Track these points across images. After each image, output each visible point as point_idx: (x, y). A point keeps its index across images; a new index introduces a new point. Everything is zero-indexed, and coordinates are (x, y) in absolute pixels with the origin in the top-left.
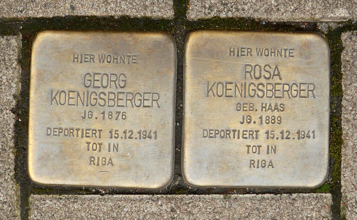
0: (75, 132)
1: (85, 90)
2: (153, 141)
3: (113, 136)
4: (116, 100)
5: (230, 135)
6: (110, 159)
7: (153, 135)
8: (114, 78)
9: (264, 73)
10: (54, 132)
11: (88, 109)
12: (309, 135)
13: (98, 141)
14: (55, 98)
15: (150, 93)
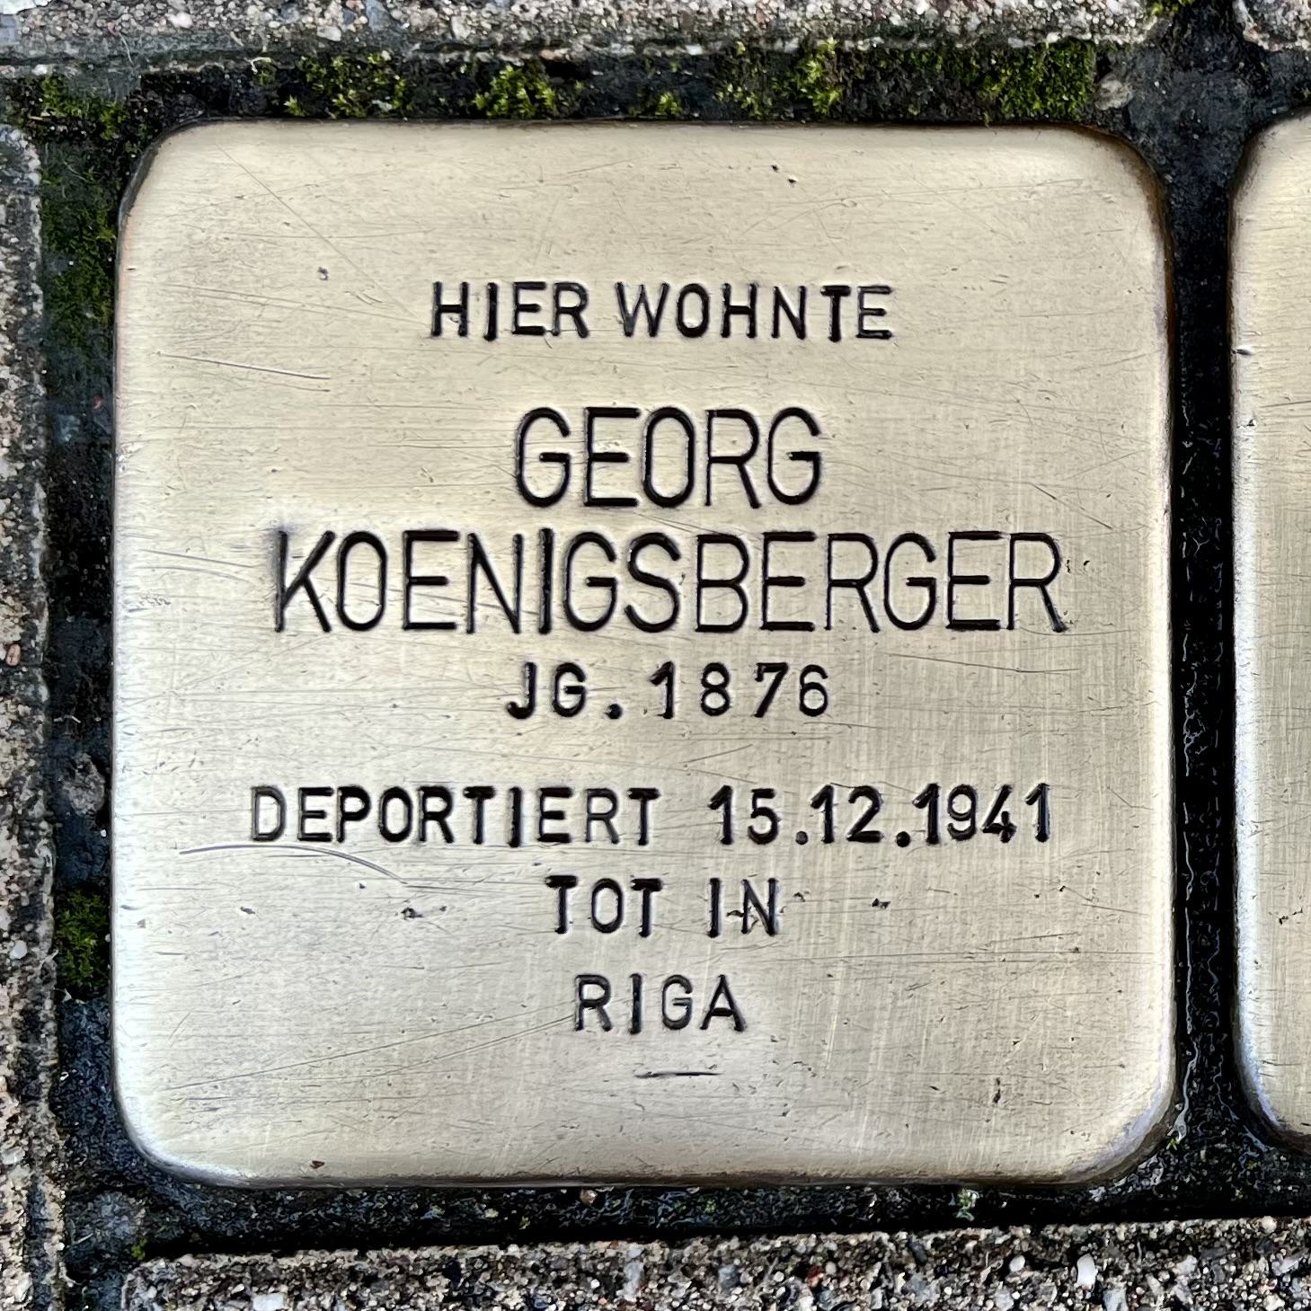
0: (463, 809)
1: (530, 524)
3: (739, 826)
4: (751, 586)
5: (449, 820)
6: (723, 987)
8: (732, 439)
10: (306, 815)
11: (562, 645)
12: (1005, 815)
13: (627, 866)
14: (303, 580)
15: (993, 536)
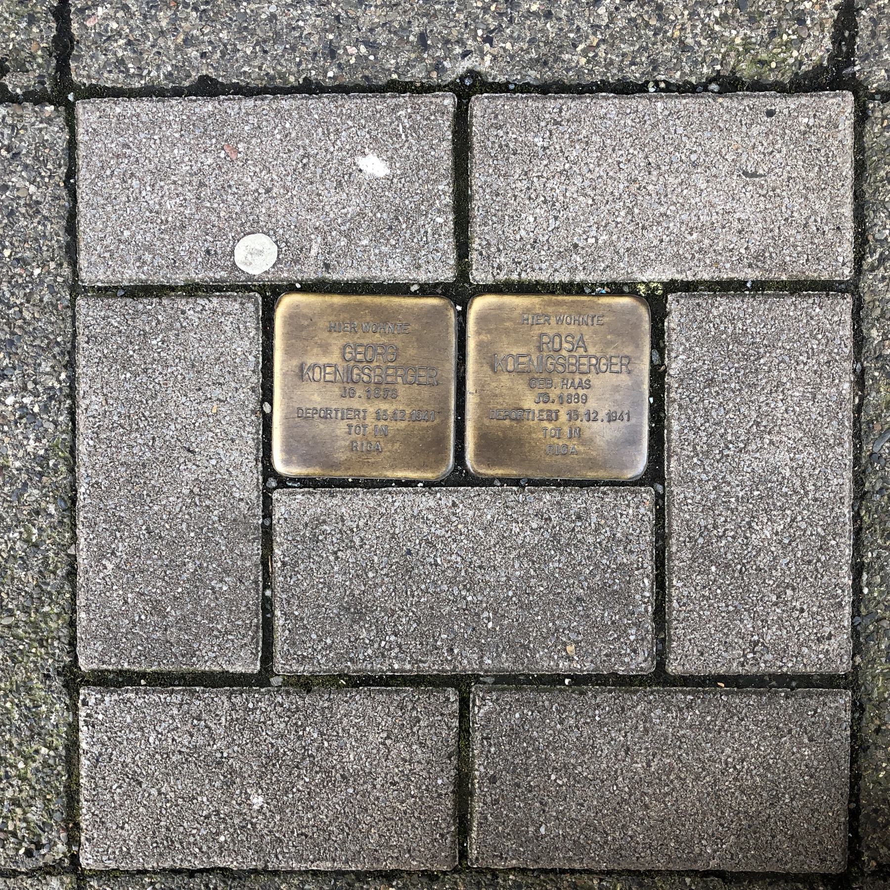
2: (625, 422)
7: (626, 417)
9: (565, 345)
